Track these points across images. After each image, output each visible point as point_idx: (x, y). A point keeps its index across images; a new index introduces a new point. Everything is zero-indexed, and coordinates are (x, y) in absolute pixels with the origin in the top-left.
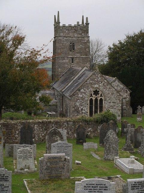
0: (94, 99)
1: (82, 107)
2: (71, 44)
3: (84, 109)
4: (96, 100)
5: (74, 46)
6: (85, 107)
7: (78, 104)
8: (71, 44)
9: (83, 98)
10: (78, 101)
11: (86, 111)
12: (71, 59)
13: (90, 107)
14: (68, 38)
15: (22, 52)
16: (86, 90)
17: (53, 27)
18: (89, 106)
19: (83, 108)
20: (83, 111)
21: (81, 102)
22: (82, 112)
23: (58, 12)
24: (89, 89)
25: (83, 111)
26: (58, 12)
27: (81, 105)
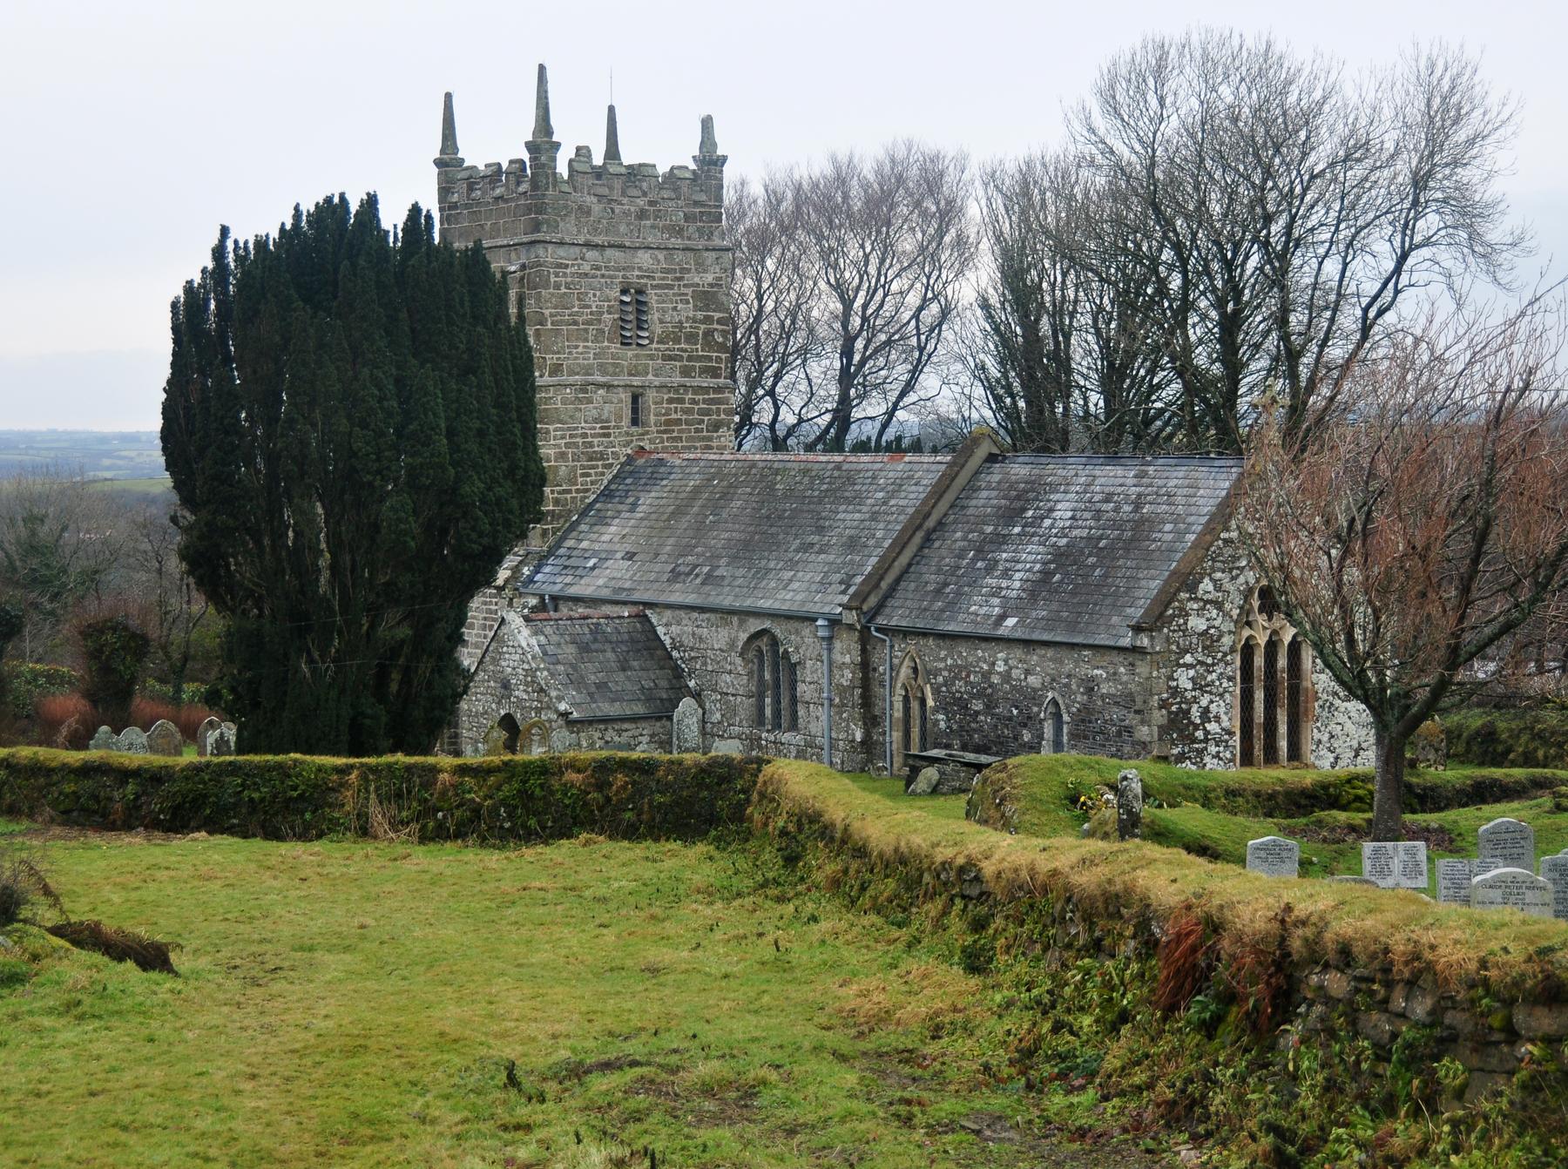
0: (1262, 640)
1: (1204, 702)
2: (627, 299)
3: (1213, 707)
4: (1272, 646)
5: (641, 306)
6: (1221, 695)
7: (1184, 679)
8: (627, 299)
9: (1209, 641)
10: (1188, 659)
11: (1226, 724)
12: (625, 396)
13: (1243, 691)
14: (609, 252)
15: (392, 218)
16: (1227, 586)
17: (169, 335)
18: (1238, 692)
19: (1212, 702)
20: (1212, 727)
21: (1201, 663)
22: (1207, 732)
23: (542, 68)
24: (1241, 579)
25: (1212, 727)
26: (542, 68)
27: (1201, 688)
